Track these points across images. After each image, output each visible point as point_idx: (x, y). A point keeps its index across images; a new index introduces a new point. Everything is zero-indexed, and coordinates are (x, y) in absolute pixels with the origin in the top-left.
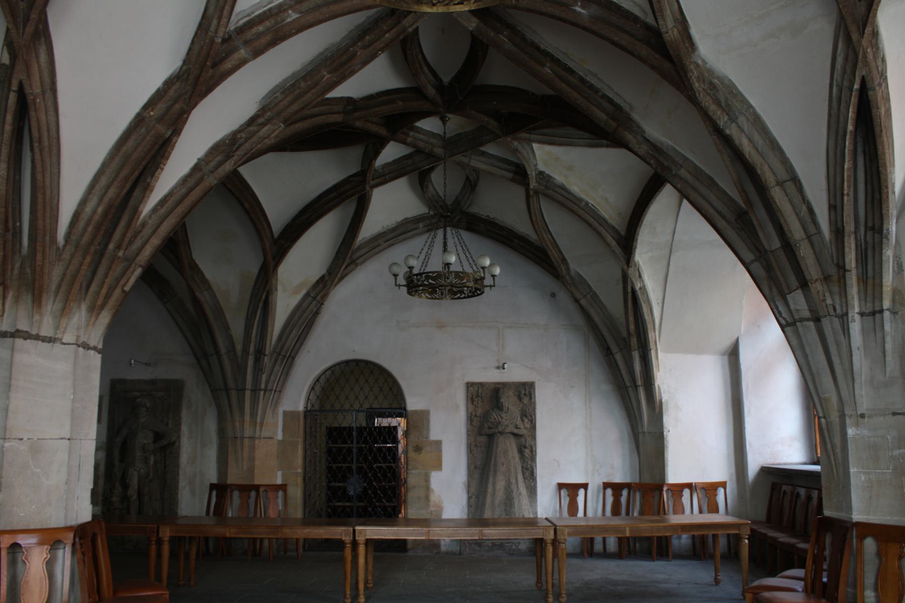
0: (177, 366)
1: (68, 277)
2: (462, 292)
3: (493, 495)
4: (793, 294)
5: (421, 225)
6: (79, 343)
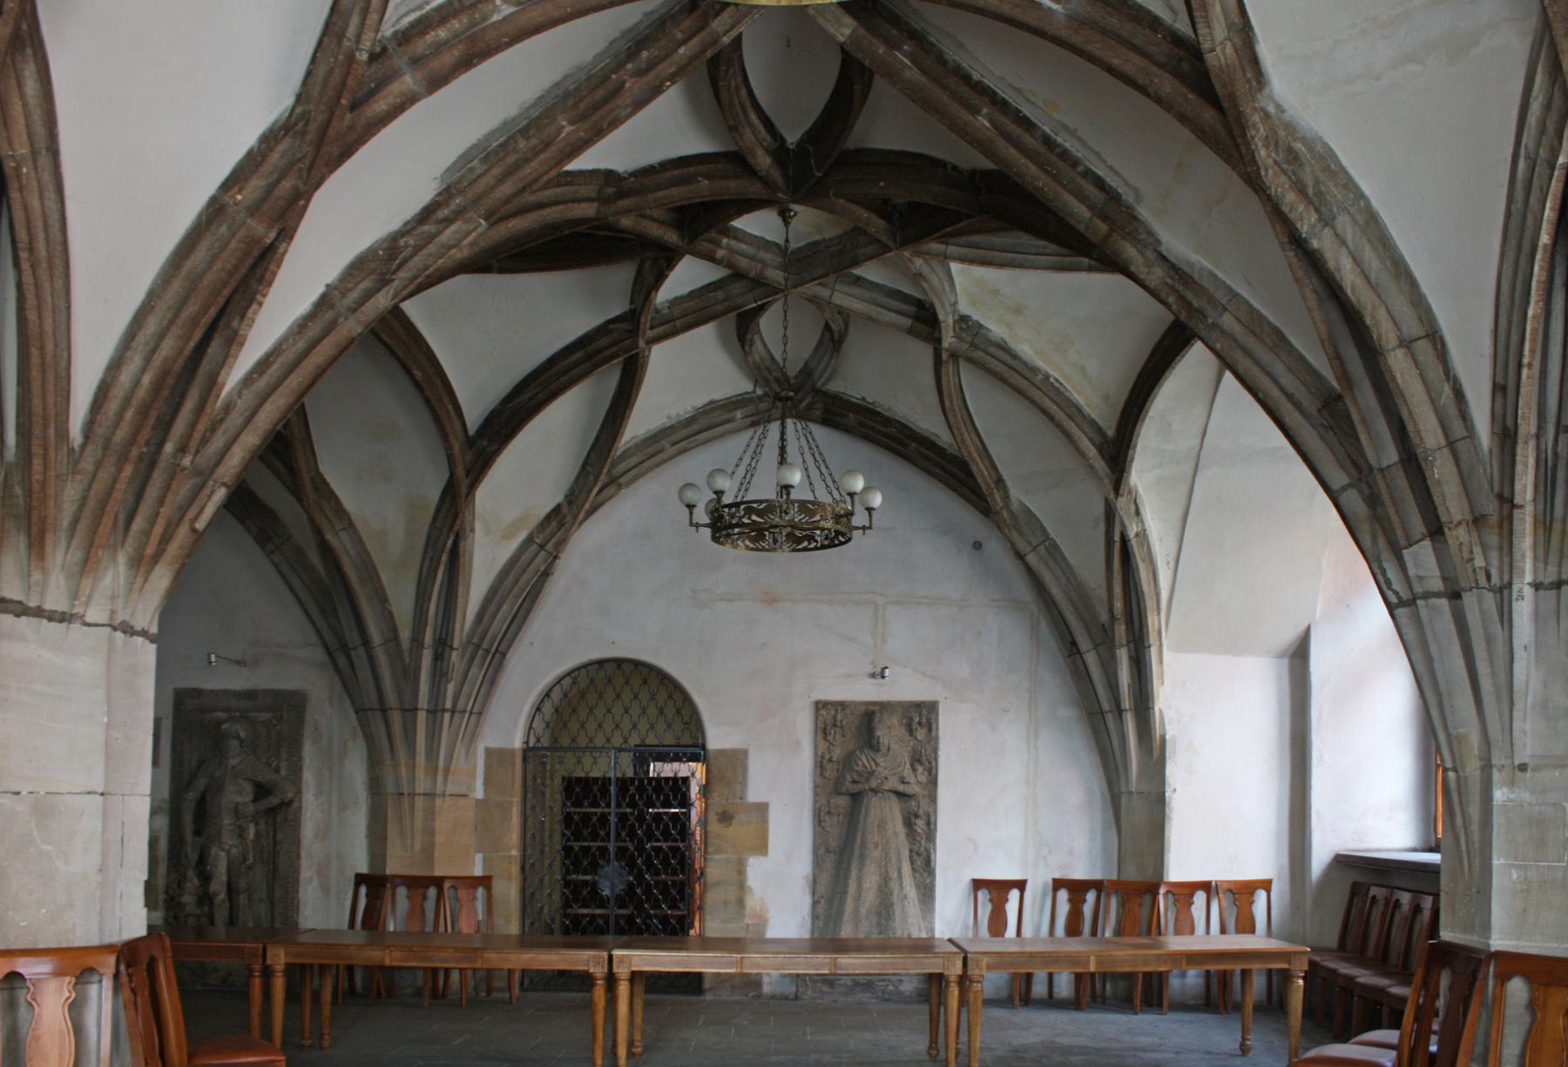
0: (298, 669)
1: (92, 503)
2: (811, 538)
3: (858, 898)
5: (739, 414)
6: (116, 623)
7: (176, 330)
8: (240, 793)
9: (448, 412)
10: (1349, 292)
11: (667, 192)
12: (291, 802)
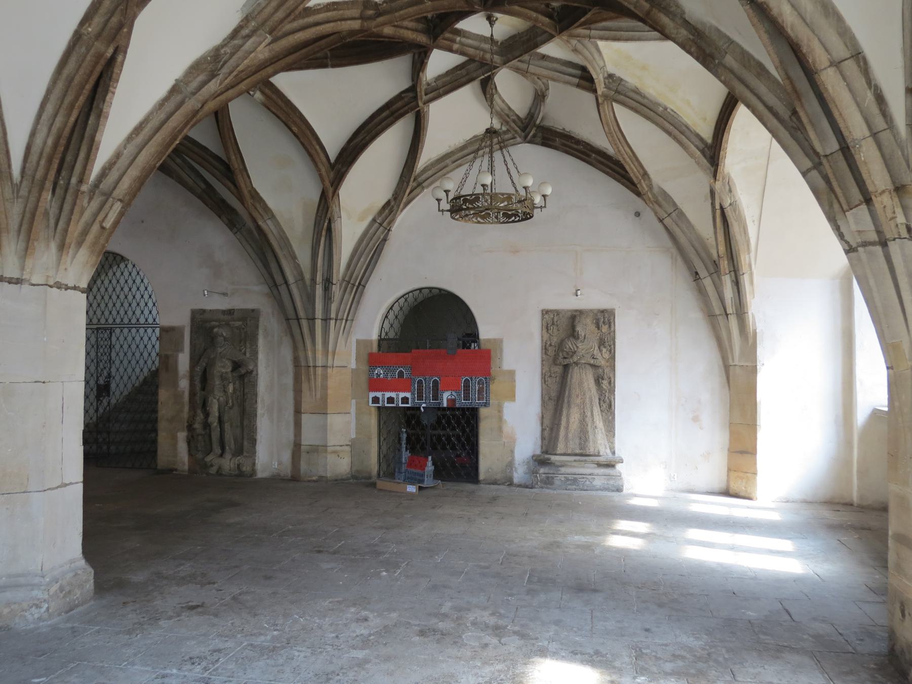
1: (28, 215)
2: (516, 215)
3: (567, 428)
4: (854, 210)
6: (51, 283)
7: (62, 112)
8: (224, 367)
9: (316, 150)
10: (789, 30)
11: (406, 10)
12: (252, 372)
